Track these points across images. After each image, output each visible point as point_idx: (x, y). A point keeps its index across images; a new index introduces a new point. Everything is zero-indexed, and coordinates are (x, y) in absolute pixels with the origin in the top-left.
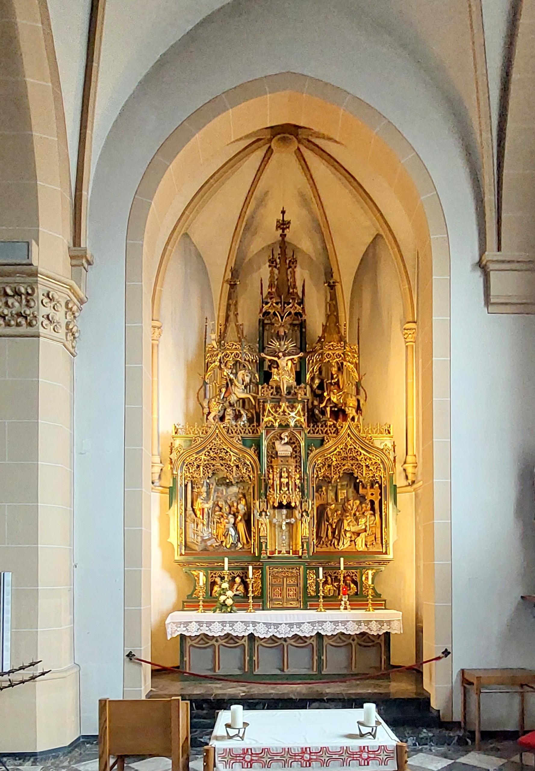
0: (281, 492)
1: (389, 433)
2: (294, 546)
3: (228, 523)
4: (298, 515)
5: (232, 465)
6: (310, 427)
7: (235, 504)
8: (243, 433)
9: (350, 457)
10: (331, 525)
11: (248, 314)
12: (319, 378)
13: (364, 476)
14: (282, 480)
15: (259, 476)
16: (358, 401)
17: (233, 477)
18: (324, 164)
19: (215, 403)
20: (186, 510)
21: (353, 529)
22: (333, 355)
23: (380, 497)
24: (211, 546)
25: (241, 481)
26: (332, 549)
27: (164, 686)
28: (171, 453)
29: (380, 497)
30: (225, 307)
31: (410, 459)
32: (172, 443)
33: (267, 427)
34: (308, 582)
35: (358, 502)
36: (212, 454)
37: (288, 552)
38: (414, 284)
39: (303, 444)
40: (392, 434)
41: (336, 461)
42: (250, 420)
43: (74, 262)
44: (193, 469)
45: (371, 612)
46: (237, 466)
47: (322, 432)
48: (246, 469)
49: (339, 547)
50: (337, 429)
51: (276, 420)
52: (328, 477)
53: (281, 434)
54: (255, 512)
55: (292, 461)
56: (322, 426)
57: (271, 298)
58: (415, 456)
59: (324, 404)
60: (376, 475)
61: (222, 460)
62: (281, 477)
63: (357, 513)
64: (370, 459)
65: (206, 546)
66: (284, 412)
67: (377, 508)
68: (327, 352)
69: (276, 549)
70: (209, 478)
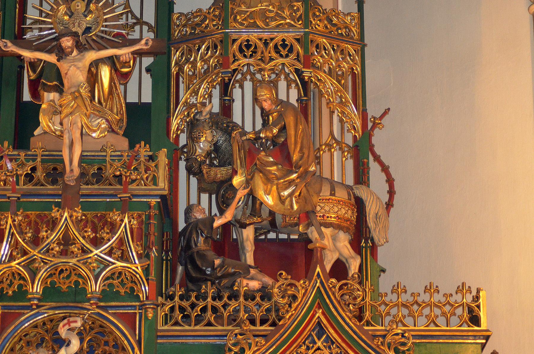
1: (475, 320)
18: (261, 178)
22: (266, 44)
40: (484, 326)
43: (60, 153)
47: (219, 318)
51: (33, 274)
56: (218, 297)
66: (66, 241)
68: (244, 36)
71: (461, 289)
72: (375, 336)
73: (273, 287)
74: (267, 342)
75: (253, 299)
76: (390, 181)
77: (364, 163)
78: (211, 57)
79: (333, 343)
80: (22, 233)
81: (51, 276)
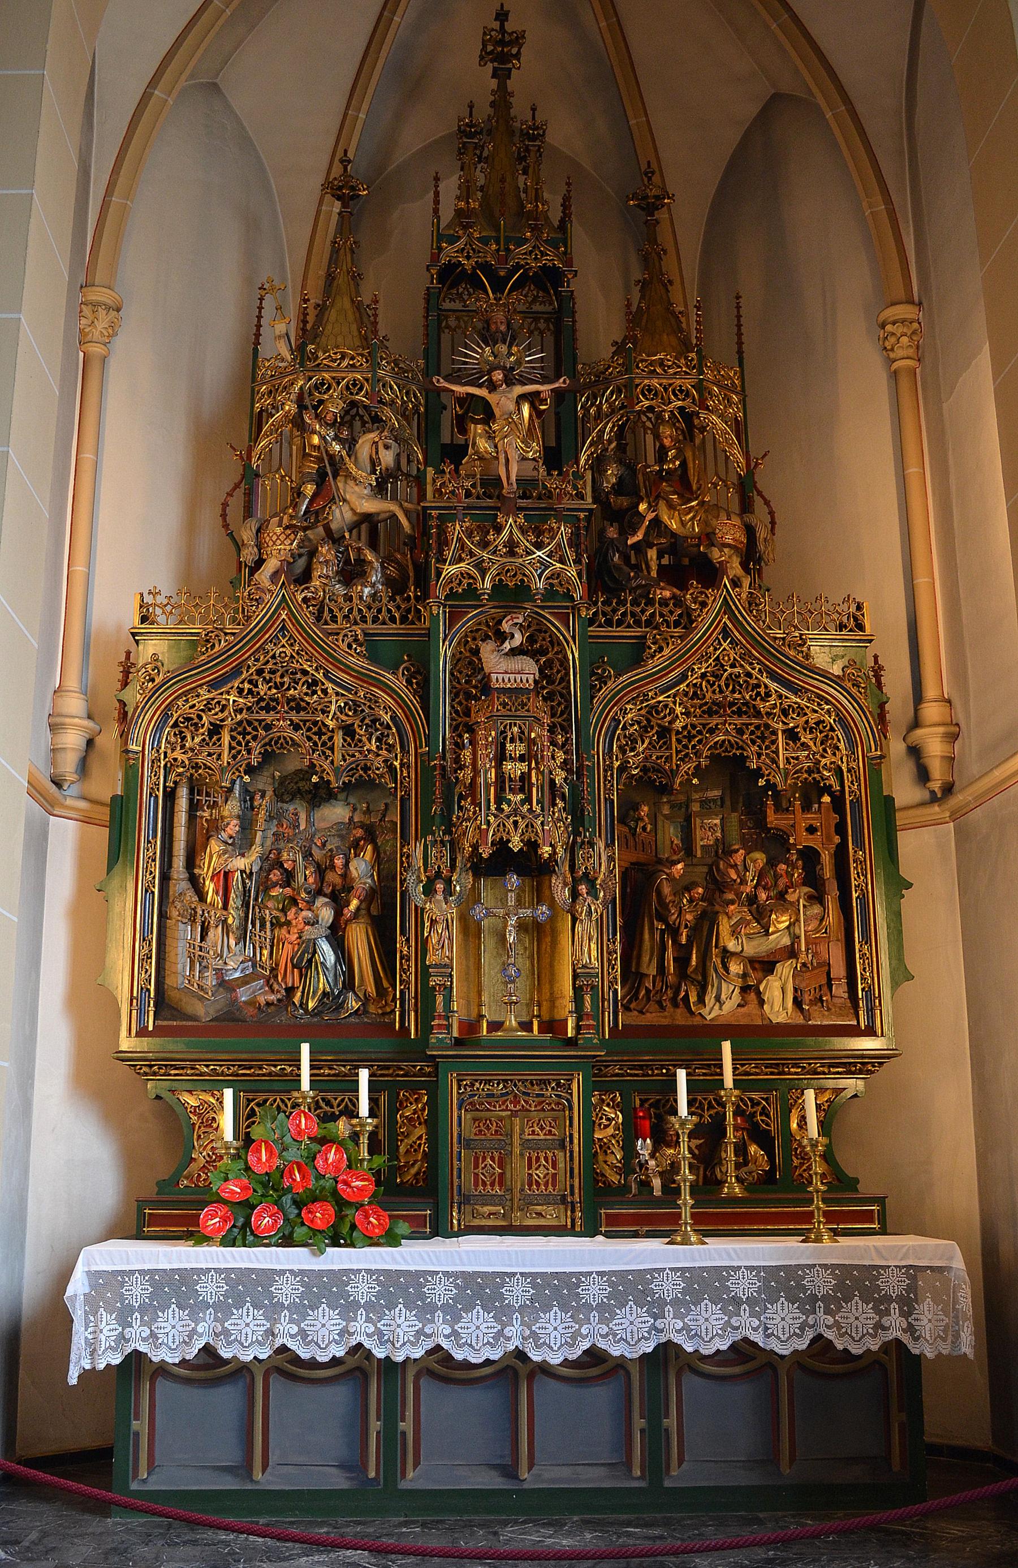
0: (505, 807)
1: (861, 627)
2: (545, 1005)
3: (313, 923)
4: (562, 894)
5: (331, 724)
6: (595, 603)
7: (339, 862)
8: (369, 620)
9: (732, 704)
10: (675, 933)
11: (397, 280)
12: (620, 462)
13: (782, 762)
14: (508, 766)
15: (424, 759)
16: (750, 531)
17: (334, 764)
19: (278, 530)
20: (165, 878)
21: (752, 948)
23: (837, 839)
24: (252, 1003)
25: (361, 784)
26: (680, 1017)
27: (44, 1534)
28: (125, 684)
29: (837, 839)
30: (321, 283)
31: (932, 711)
32: (128, 654)
33: (451, 595)
34: (597, 1135)
35: (760, 858)
36: (262, 688)
37: (527, 1026)
38: (903, 202)
39: (573, 653)
41: (687, 714)
42: (396, 586)
44: (197, 740)
45: (826, 1242)
46: (349, 731)
48: (378, 739)
49: (704, 1012)
50: (688, 613)
51: (483, 573)
52: (658, 770)
53: (500, 622)
54: (411, 878)
55: (538, 706)
56: (635, 603)
57: (465, 227)
58: (949, 701)
59: (639, 536)
60: (823, 761)
61: (298, 709)
62: (501, 757)
63: (763, 896)
64: (801, 711)
65: (234, 1001)
66: (511, 546)
67: (830, 879)
69: (481, 1016)
70: (250, 770)
71: (847, 600)
72: (776, 638)
73: (684, 596)
74: (682, 641)
75: (667, 605)
76: (772, 513)
77: (749, 497)
78: (616, 400)
79: (737, 645)
80: (470, 536)
81: (498, 574)
